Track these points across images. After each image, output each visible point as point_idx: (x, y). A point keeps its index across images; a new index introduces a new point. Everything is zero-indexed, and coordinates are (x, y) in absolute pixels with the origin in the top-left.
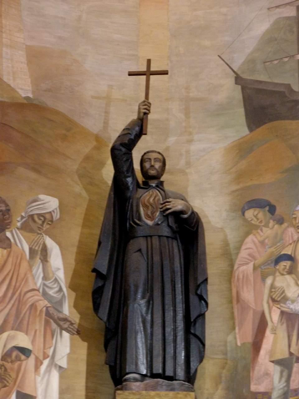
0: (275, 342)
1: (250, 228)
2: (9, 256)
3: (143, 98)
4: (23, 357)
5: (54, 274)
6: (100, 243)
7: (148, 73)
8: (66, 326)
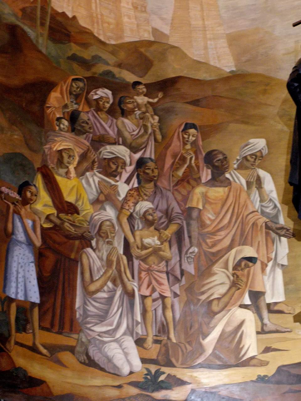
2: (230, 191)
4: (251, 264)
5: (268, 195)
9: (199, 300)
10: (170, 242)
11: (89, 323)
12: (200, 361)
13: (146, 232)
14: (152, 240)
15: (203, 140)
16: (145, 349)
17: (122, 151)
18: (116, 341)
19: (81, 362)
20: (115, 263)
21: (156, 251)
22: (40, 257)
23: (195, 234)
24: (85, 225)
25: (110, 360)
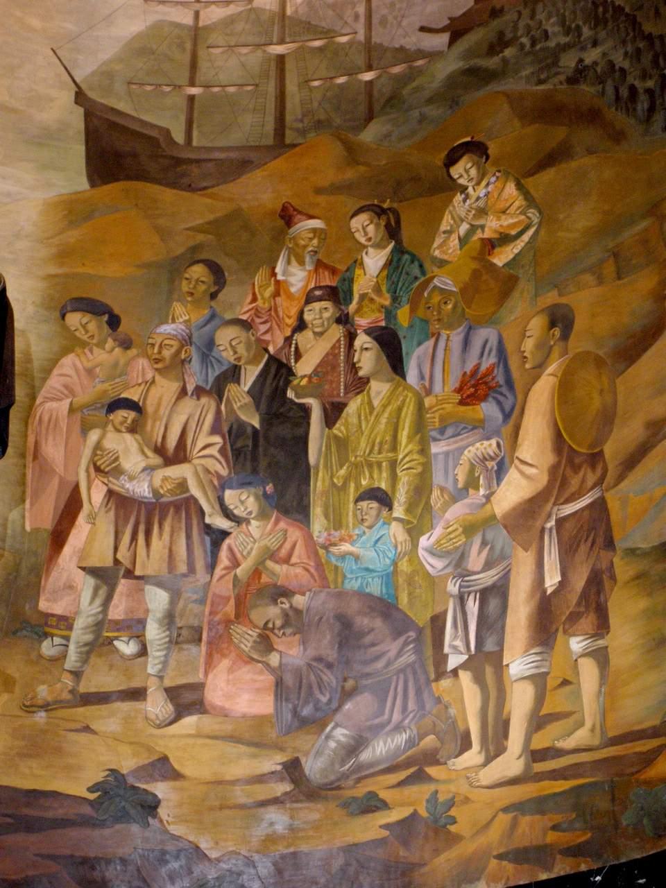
1: (71, 344)
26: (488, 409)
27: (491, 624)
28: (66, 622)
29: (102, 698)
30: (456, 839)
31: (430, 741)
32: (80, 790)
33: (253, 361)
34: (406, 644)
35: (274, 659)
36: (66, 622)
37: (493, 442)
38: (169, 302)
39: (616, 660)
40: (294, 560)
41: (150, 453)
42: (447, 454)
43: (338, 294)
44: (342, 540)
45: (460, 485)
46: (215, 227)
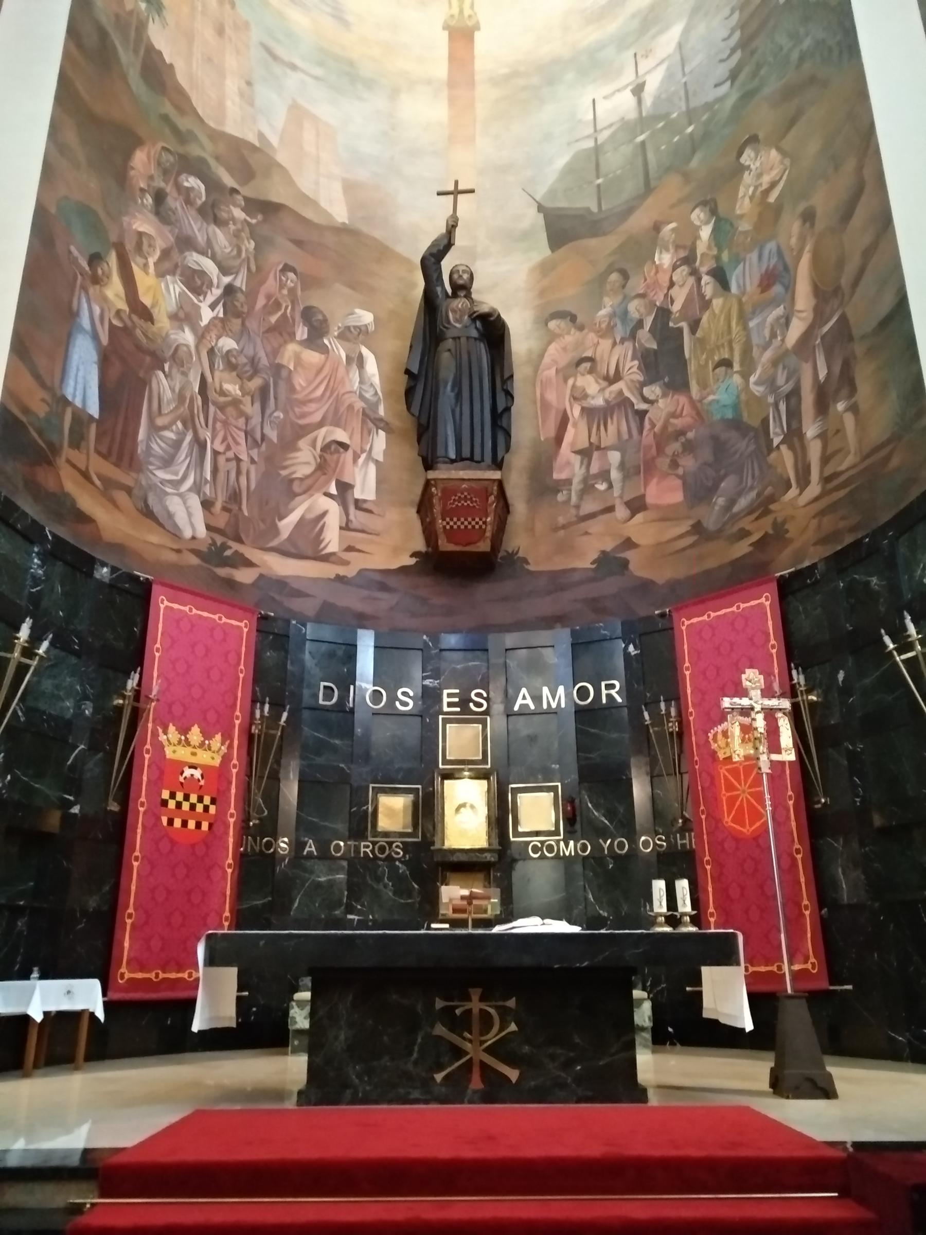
0: (576, 434)
1: (552, 337)
2: (327, 358)
3: (451, 212)
4: (342, 450)
5: (369, 379)
6: (411, 347)
7: (456, 192)
8: (382, 425)
9: (280, 475)
10: (252, 397)
11: (151, 464)
12: (274, 543)
13: (226, 375)
14: (233, 388)
15: (302, 290)
16: (212, 514)
17: (209, 266)
18: (181, 495)
19: (137, 509)
20: (188, 401)
21: (236, 403)
22: (105, 360)
23: (282, 396)
24: (159, 341)
25: (170, 516)
26: (777, 289)
27: (794, 414)
28: (569, 482)
29: (592, 516)
30: (791, 541)
31: (769, 490)
32: (588, 565)
33: (649, 314)
34: (750, 440)
35: (680, 471)
36: (569, 482)
37: (782, 306)
38: (601, 298)
39: (863, 407)
40: (685, 413)
41: (601, 381)
42: (758, 324)
43: (689, 260)
44: (708, 394)
45: (768, 339)
46: (621, 248)
